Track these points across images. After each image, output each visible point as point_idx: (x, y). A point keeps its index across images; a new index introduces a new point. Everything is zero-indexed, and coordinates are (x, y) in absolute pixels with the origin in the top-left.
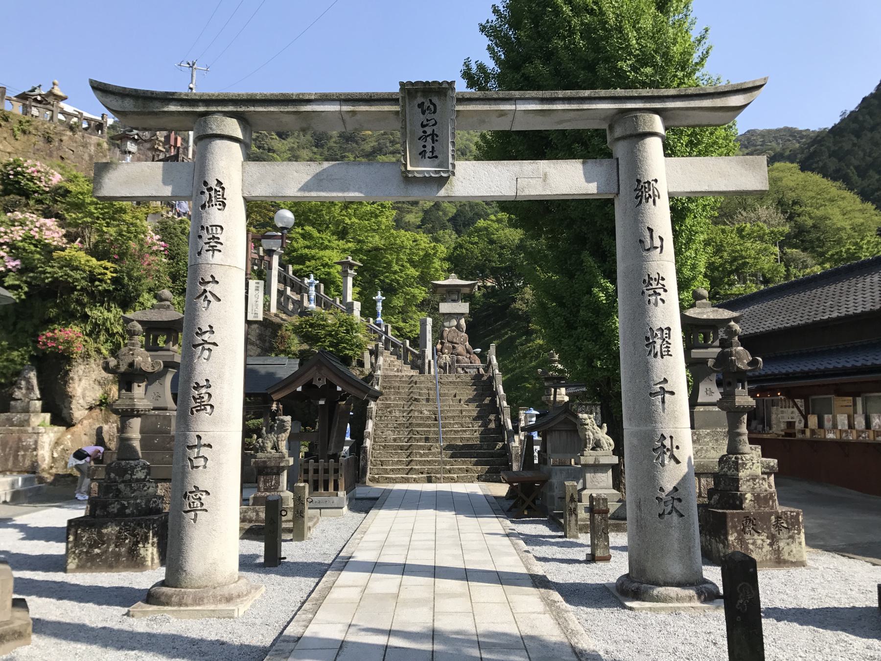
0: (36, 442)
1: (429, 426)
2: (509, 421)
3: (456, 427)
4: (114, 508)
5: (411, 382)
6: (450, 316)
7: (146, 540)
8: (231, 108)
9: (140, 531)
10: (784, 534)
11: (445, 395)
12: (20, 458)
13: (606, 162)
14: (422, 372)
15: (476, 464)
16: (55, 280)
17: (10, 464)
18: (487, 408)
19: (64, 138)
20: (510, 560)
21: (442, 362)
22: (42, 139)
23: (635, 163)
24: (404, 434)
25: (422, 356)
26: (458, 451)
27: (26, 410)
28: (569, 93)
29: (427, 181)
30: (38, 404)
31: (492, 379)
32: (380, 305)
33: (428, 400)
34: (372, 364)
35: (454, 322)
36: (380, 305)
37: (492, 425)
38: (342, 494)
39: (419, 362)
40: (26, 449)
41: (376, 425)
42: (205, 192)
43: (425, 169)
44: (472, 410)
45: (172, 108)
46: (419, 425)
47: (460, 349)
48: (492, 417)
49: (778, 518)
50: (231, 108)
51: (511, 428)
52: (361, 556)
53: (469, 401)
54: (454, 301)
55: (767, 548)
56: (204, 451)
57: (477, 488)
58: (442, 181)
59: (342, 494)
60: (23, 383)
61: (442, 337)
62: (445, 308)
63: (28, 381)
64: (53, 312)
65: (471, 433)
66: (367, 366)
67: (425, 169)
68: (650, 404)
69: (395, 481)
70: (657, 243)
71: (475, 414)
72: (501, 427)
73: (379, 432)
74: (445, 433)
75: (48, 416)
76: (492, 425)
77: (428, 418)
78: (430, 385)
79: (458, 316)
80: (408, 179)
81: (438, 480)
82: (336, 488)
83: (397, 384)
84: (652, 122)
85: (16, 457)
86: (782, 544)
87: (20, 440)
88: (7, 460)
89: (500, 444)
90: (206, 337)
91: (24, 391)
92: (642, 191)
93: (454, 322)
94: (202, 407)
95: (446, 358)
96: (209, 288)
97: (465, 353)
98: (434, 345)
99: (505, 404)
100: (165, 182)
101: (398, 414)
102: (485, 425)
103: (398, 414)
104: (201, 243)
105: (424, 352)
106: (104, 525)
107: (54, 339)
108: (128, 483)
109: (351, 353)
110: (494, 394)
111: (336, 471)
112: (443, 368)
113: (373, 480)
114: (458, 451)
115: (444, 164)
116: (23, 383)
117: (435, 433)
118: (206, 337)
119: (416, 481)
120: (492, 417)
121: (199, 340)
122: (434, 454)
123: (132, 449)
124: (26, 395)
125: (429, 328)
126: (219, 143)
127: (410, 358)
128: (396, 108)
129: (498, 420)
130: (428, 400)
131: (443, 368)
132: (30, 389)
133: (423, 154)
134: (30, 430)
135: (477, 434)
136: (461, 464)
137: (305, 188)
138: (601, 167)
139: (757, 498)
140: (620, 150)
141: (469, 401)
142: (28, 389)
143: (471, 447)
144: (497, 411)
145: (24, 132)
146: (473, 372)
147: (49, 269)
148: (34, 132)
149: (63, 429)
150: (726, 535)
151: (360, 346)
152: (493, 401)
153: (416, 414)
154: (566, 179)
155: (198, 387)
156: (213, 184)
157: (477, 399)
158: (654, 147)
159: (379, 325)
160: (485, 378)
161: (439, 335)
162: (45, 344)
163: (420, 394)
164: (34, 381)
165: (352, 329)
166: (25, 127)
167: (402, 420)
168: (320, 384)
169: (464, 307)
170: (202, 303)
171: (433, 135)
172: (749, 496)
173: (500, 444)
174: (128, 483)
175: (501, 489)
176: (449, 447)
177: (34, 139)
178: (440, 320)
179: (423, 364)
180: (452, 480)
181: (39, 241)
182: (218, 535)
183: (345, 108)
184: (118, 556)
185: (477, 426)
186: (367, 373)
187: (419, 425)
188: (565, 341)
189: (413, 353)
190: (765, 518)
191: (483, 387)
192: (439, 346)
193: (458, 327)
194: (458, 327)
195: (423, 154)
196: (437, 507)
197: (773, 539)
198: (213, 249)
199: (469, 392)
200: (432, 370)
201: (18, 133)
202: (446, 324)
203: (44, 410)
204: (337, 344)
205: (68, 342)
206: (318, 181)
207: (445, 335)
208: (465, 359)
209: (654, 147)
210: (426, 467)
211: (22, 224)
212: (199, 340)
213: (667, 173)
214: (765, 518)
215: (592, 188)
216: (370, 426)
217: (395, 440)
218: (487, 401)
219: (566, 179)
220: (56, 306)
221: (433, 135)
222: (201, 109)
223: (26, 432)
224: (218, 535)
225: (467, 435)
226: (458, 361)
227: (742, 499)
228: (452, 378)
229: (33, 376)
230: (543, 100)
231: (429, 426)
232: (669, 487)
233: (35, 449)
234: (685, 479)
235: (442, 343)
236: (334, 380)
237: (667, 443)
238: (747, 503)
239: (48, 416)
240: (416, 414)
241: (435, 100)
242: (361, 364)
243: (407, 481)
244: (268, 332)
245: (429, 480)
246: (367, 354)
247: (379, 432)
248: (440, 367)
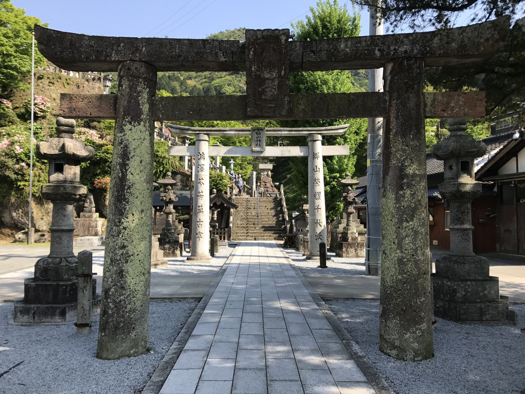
0: (96, 224)
1: (255, 219)
2: (287, 217)
3: (266, 219)
4: (167, 240)
5: (247, 201)
6: (264, 170)
7: (177, 249)
8: (205, 132)
9: (175, 246)
10: (359, 248)
11: (261, 206)
12: (91, 231)
13: (306, 147)
14: (251, 196)
15: (274, 234)
16: (101, 158)
17: (86, 233)
18: (279, 212)
19: (85, 85)
20: (282, 255)
21: (260, 191)
22: (75, 86)
23: (313, 148)
24: (245, 222)
25: (251, 189)
26: (267, 229)
27: (90, 211)
28: (296, 129)
29: (258, 152)
30: (94, 209)
31: (281, 199)
32: (232, 165)
33: (254, 208)
34: (230, 193)
35: (266, 173)
36: (232, 165)
37: (281, 219)
38: (226, 241)
39: (250, 191)
40: (92, 227)
41: (233, 218)
42: (199, 155)
43: (257, 149)
44: (273, 212)
45: (190, 132)
46: (251, 219)
47: (268, 185)
48: (281, 215)
49: (358, 244)
50: (205, 132)
51: (287, 219)
52: (236, 254)
53: (271, 209)
54: (266, 163)
55: (354, 252)
56: (201, 223)
57: (274, 242)
58: (262, 152)
59: (226, 241)
60: (88, 200)
61: (260, 180)
62: (261, 166)
63: (90, 200)
64: (99, 171)
65: (272, 222)
66: (229, 194)
67: (257, 149)
68: (315, 211)
69: (242, 240)
70: (318, 170)
71: (274, 214)
72: (284, 219)
73: (235, 221)
74: (261, 222)
75: (98, 214)
76: (281, 219)
77: (255, 216)
78: (255, 202)
79: (267, 170)
80: (253, 151)
81: (259, 239)
82: (224, 239)
83: (241, 202)
84: (318, 137)
85: (89, 230)
86: (358, 251)
87: (90, 223)
88: (85, 232)
89: (284, 226)
90: (201, 194)
91: (88, 204)
92: (314, 156)
93: (266, 173)
94: (200, 212)
95: (262, 189)
96: (201, 181)
97: (270, 187)
98: (257, 183)
99: (286, 210)
100: (187, 152)
101: (242, 214)
102: (278, 218)
103: (242, 214)
104: (199, 169)
105: (252, 187)
106: (165, 245)
107: (100, 183)
108: (171, 233)
109: (222, 188)
110: (282, 206)
111: (224, 234)
112: (260, 194)
113: (233, 239)
114: (267, 229)
115: (262, 148)
116: (88, 200)
117: (257, 222)
118: (201, 194)
119: (250, 240)
120: (281, 215)
121: (199, 194)
122: (257, 230)
123: (170, 223)
124: (89, 205)
125: (254, 176)
126: (202, 142)
127: (246, 189)
128: (250, 133)
129: (283, 217)
130: (254, 208)
131: (260, 194)
132: (91, 203)
133: (257, 145)
134: (93, 219)
135: (274, 222)
136: (268, 233)
137: (225, 153)
138: (304, 148)
139: (352, 239)
140: (310, 144)
141: (271, 209)
142: (90, 203)
143: (272, 227)
144: (283, 213)
145: (68, 84)
146: (274, 196)
147: (98, 154)
148: (72, 83)
149: (104, 219)
150: (342, 249)
151: (226, 186)
152: (281, 209)
153: (250, 214)
154: (295, 151)
155: (199, 206)
156: (201, 153)
157: (275, 208)
158: (319, 144)
159: (232, 175)
160: (278, 199)
161: (258, 179)
162: (97, 185)
163: (251, 206)
164: (93, 200)
165: (223, 179)
166: (68, 81)
167: (244, 217)
168: (218, 203)
169: (270, 166)
170: (199, 185)
171: (260, 140)
172: (350, 238)
173: (284, 226)
174: (171, 233)
175: (282, 242)
176: (263, 227)
177: (72, 87)
178: (259, 172)
179: (252, 192)
180: (264, 239)
181: (91, 141)
182: (203, 244)
183: (236, 133)
184: (169, 253)
185: (274, 219)
186: (229, 197)
187: (251, 219)
188: (303, 189)
189: (247, 187)
190: (354, 244)
191: (278, 203)
192: (259, 184)
193: (267, 175)
194: (267, 175)
195: (257, 145)
196: (258, 246)
197: (356, 250)
198: (202, 171)
199: (272, 205)
200: (256, 195)
201: (66, 84)
202: (262, 174)
203: (96, 212)
204: (216, 185)
205: (106, 184)
206: (229, 152)
207: (261, 179)
208: (270, 190)
209: (319, 144)
210: (254, 235)
211: (84, 133)
212: (199, 194)
213: (321, 150)
214: (354, 244)
215: (302, 154)
216: (231, 218)
217: (241, 224)
218: (279, 209)
219: (295, 151)
220: (100, 168)
221: (260, 140)
222: (198, 132)
223: (92, 220)
224: (203, 244)
225: (270, 223)
226: (267, 191)
227: (348, 239)
228: (265, 199)
229: (92, 197)
230: (289, 131)
231: (255, 219)
232: (318, 232)
233: (96, 227)
234: (323, 230)
235: (260, 183)
236: (224, 202)
237: (318, 221)
238: (349, 240)
239: (98, 214)
240: (250, 214)
241: (260, 131)
242: (226, 193)
243: (247, 240)
244: (185, 178)
245: (255, 239)
246: (228, 189)
247: (235, 221)
248: (259, 193)
